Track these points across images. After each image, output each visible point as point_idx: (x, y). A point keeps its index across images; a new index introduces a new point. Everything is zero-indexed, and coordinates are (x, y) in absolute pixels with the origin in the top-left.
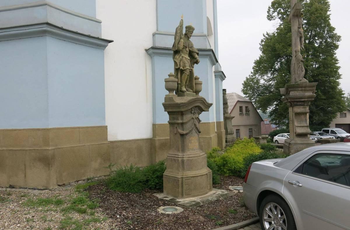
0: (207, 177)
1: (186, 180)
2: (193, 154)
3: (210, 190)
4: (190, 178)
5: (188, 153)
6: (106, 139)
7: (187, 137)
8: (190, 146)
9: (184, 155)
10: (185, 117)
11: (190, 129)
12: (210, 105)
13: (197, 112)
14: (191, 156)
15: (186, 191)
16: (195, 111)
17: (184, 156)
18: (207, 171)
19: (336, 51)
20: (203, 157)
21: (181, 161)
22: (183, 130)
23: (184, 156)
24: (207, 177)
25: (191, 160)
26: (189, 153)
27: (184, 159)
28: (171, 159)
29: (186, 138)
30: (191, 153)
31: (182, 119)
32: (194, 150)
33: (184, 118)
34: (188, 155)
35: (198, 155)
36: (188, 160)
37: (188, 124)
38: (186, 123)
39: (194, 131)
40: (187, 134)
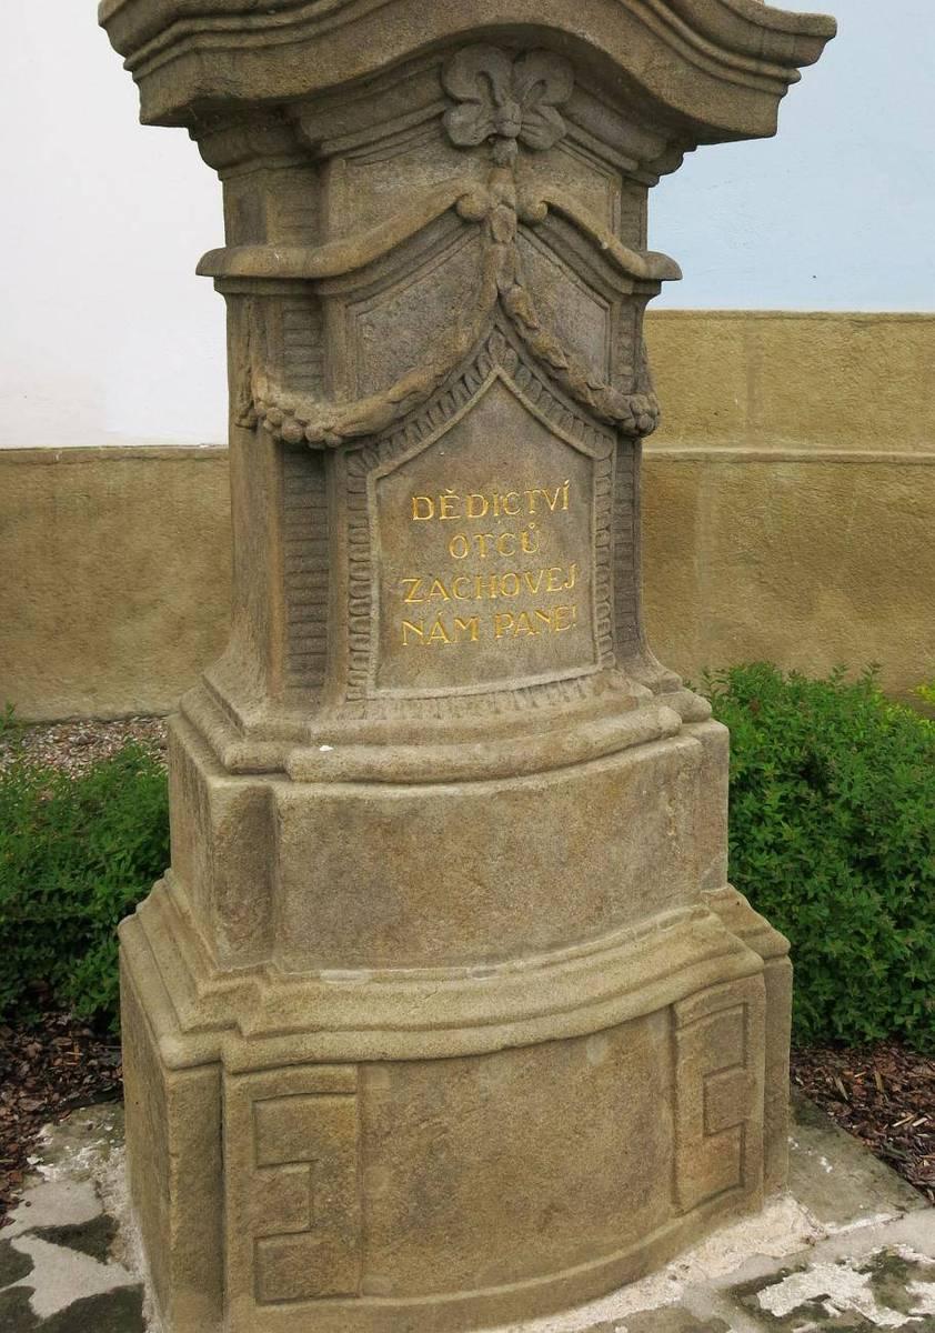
0: (673, 1040)
1: (274, 1095)
2: (445, 736)
3: (737, 1193)
4: (349, 1071)
5: (388, 706)
6: (210, 456)
7: (382, 487)
8: (430, 613)
9: (302, 739)
10: (342, 195)
11: (419, 379)
12: (789, 47)
13: (541, 138)
14: (412, 755)
15: (279, 1254)
16: (511, 110)
17: (298, 756)
18: (686, 951)
19: (33, 1300)
20: (619, 780)
21: (241, 816)
22: (322, 383)
23: (298, 756)
24: (673, 1040)
25: (391, 827)
26: (391, 719)
27: (284, 792)
28: (532, 669)
29: (358, 494)
30: (425, 719)
31: (314, 230)
32: (494, 670)
33: (335, 220)
34: (375, 740)
35: (532, 747)
36: (344, 813)
37: (385, 302)
38: (362, 280)
39: (498, 403)
40: (363, 443)
